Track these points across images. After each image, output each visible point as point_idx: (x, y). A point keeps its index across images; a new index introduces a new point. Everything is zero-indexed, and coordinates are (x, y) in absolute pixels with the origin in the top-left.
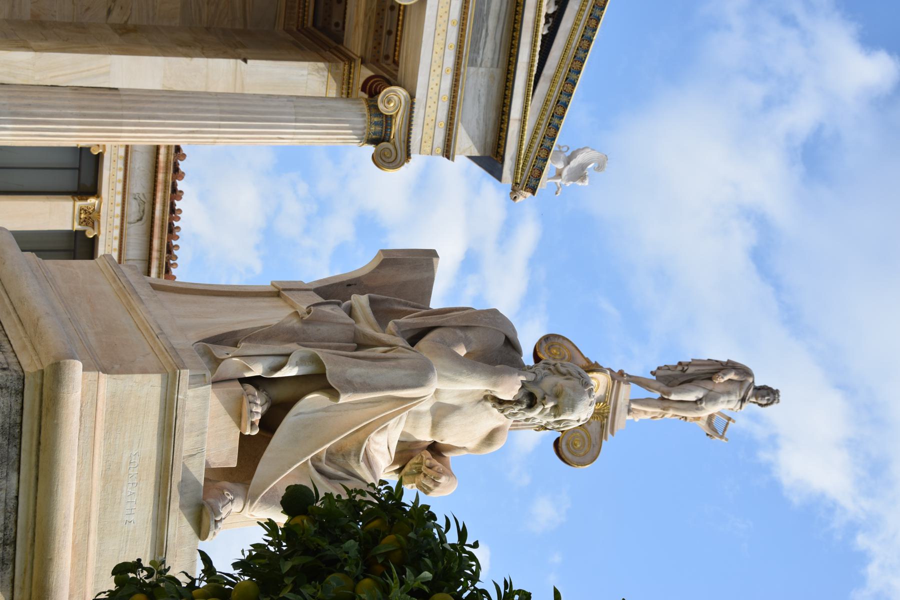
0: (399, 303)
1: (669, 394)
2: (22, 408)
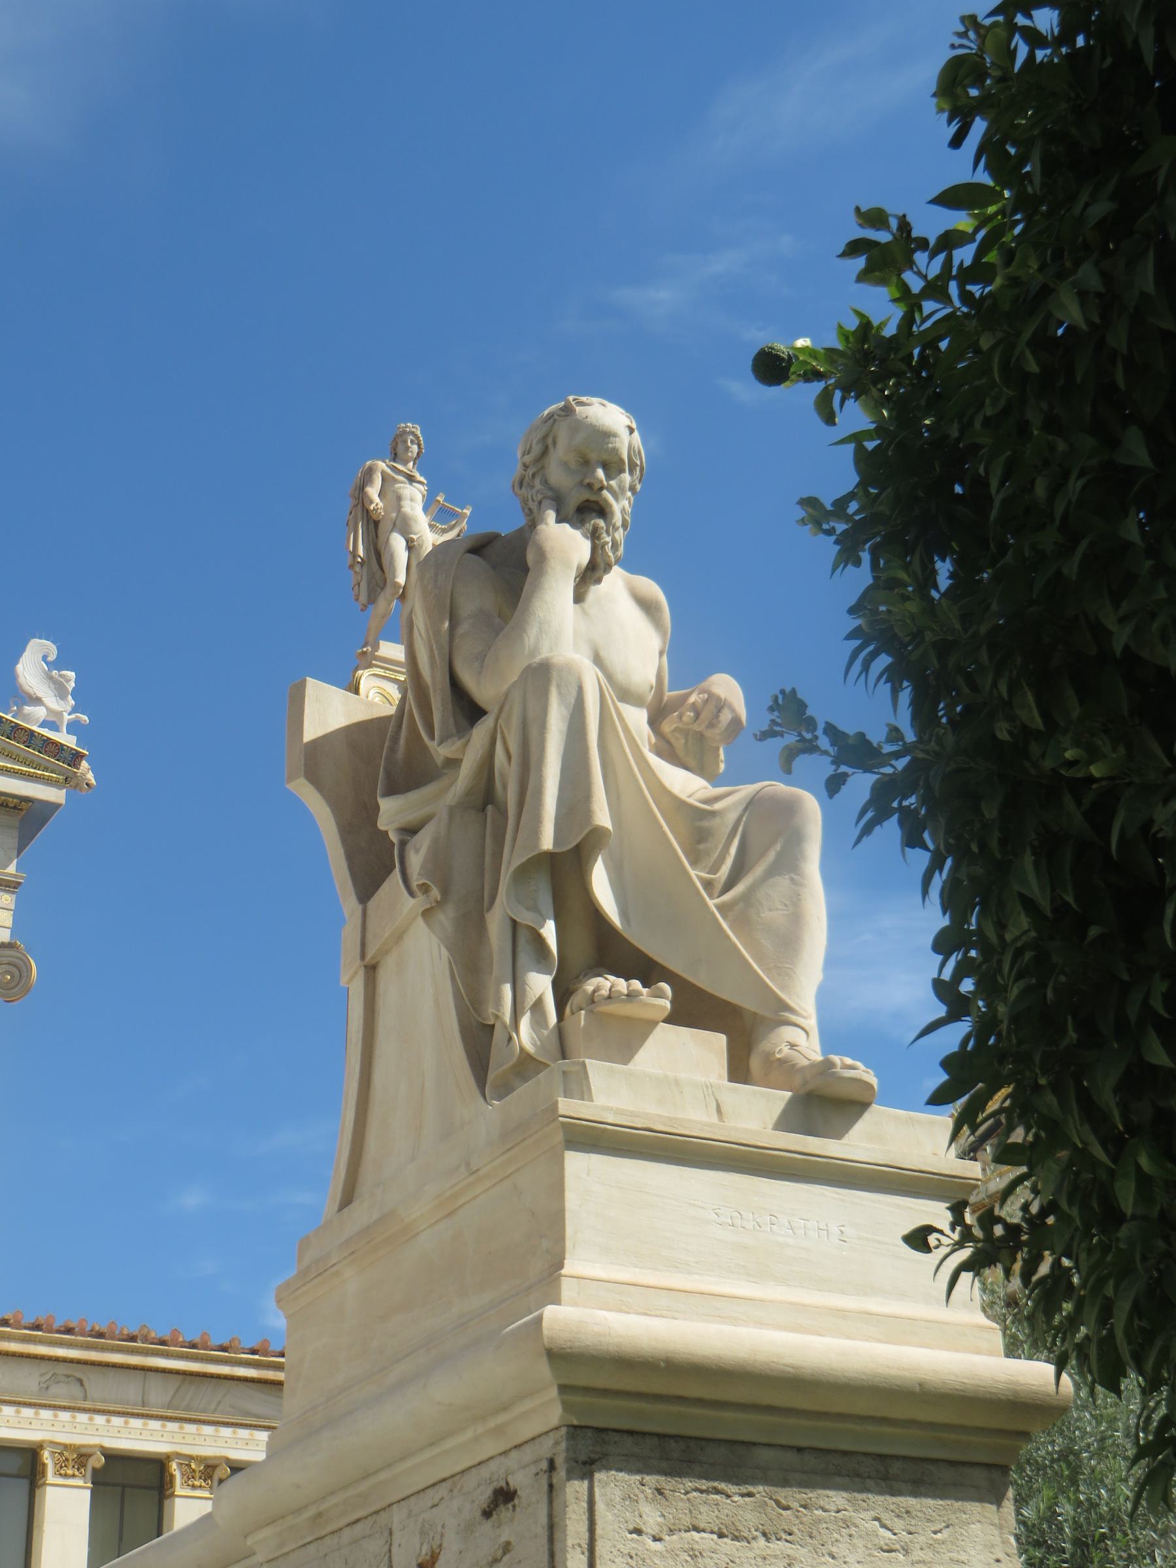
0: (393, 749)
1: (396, 585)
2: (631, 1433)
